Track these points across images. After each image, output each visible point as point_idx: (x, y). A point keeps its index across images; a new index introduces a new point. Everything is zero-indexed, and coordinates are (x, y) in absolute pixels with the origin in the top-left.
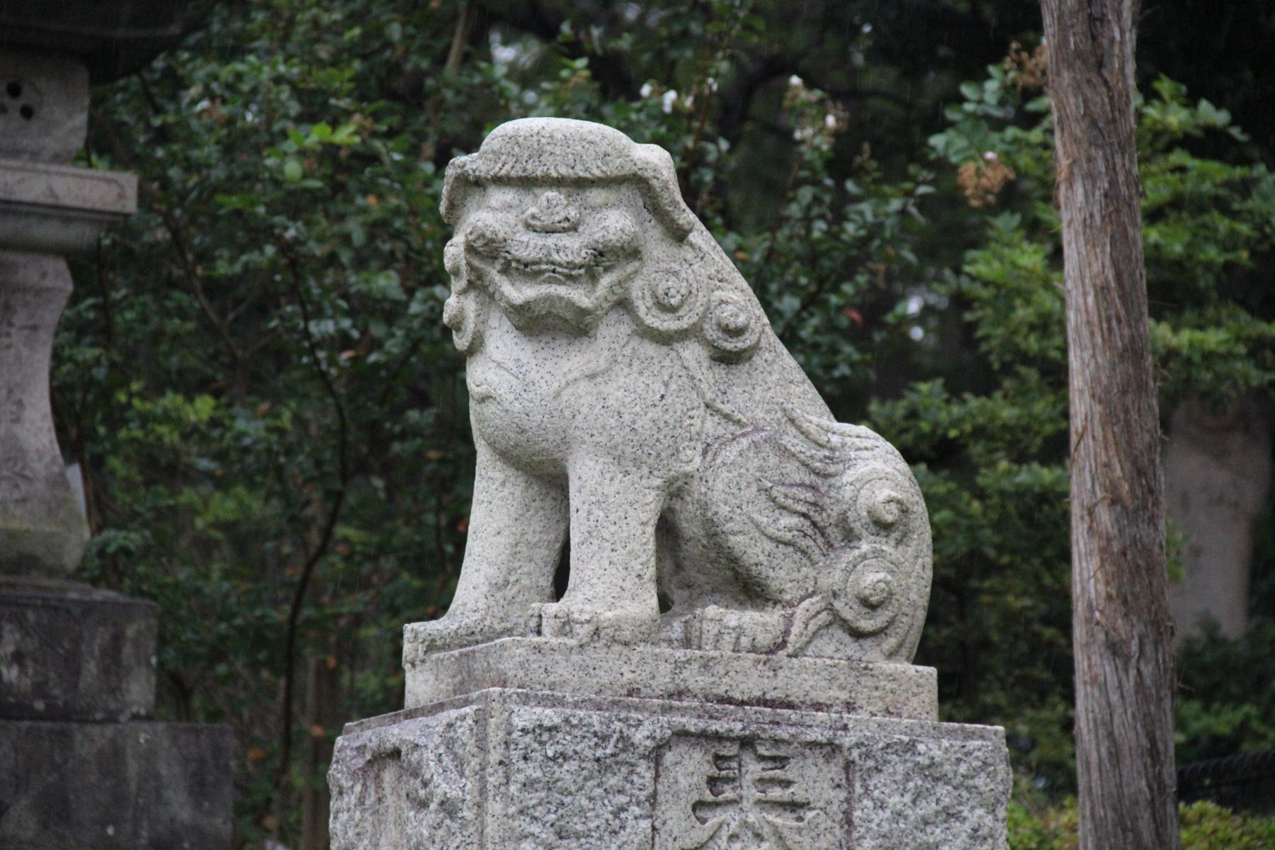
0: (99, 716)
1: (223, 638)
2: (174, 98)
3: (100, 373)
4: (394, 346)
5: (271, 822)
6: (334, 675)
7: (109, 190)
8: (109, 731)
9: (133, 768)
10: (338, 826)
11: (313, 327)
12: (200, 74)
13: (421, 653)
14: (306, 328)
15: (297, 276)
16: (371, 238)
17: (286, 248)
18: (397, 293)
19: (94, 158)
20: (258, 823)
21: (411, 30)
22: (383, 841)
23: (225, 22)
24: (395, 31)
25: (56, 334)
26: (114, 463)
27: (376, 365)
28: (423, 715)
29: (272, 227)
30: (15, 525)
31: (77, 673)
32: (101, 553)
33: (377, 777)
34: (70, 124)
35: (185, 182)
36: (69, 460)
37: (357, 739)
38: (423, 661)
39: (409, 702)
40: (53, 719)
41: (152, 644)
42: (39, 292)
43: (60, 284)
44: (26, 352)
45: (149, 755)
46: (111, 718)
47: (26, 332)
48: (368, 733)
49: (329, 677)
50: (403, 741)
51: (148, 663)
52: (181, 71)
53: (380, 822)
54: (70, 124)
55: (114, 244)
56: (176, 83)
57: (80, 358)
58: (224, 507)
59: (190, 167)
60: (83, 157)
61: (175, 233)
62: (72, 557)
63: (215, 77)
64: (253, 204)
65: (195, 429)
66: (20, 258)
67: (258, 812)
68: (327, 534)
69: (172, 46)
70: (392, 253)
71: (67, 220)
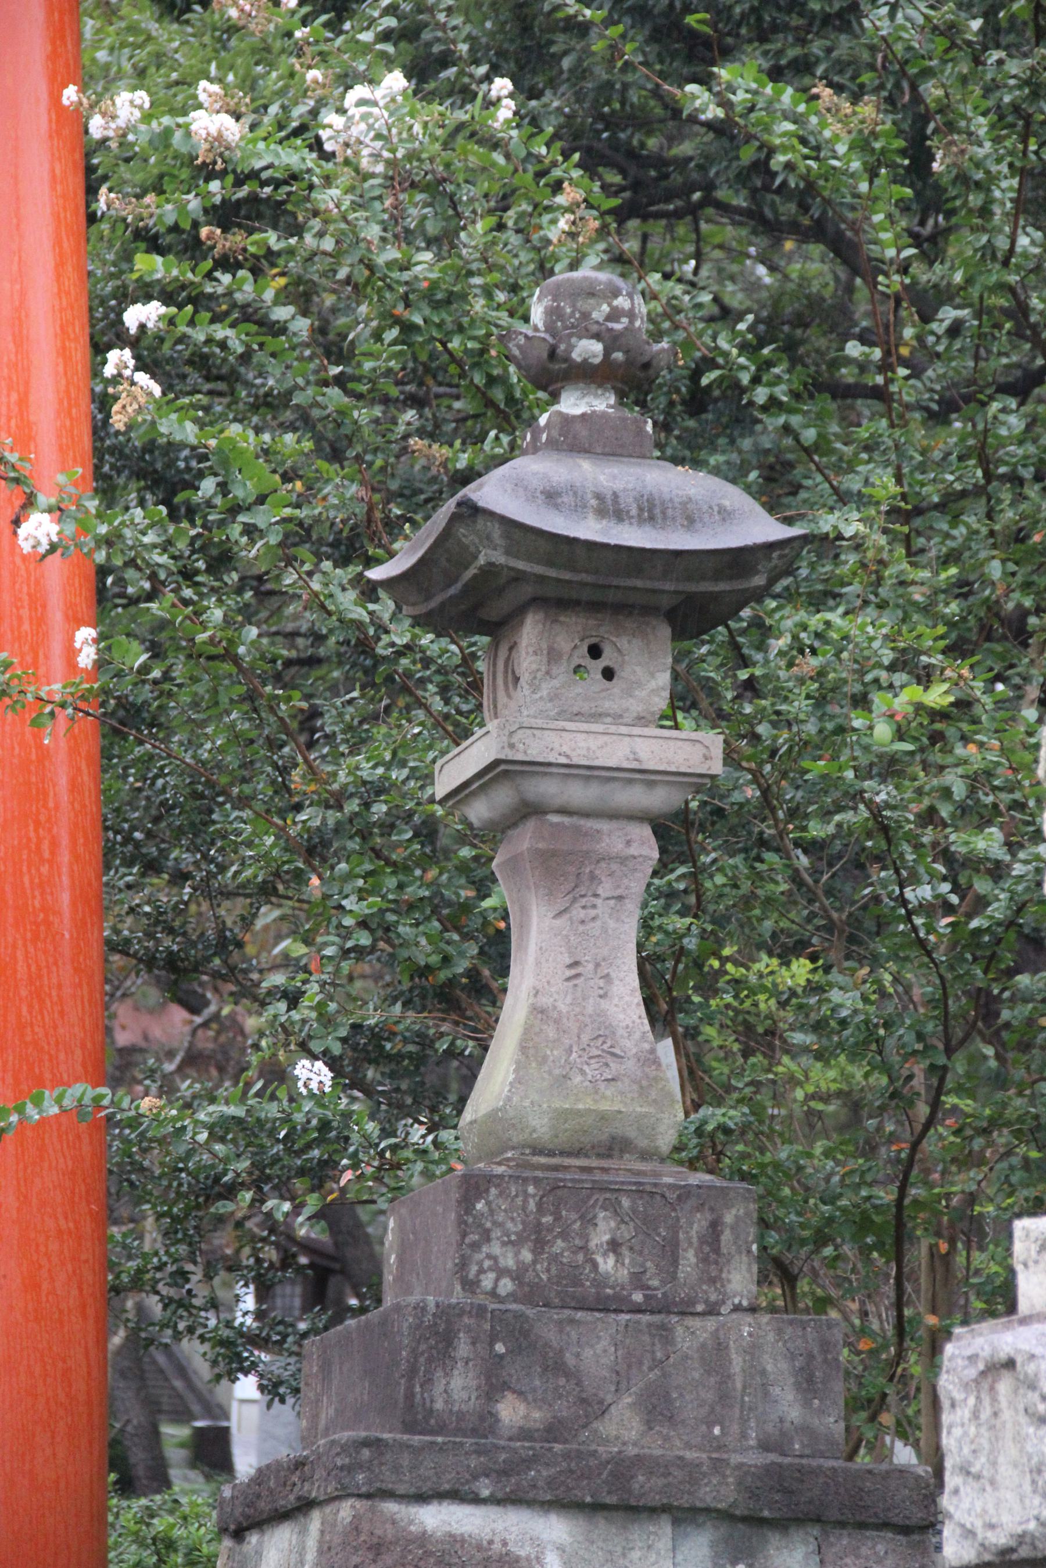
0: (700, 1308)
1: (830, 1220)
2: (761, 646)
3: (691, 943)
4: (998, 910)
5: (887, 1419)
6: (947, 1260)
7: (695, 750)
8: (711, 1323)
9: (737, 1363)
10: (952, 1442)
11: (909, 893)
12: (789, 623)
13: (1033, 1254)
14: (902, 894)
15: (889, 841)
16: (972, 790)
17: (875, 811)
18: (999, 852)
19: (680, 716)
20: (873, 1418)
21: (1011, 567)
22: (1001, 1459)
23: (812, 566)
24: (995, 570)
25: (645, 905)
26: (710, 1031)
27: (978, 932)
28: (1039, 1321)
29: (862, 791)
30: (605, 1106)
31: (675, 1262)
32: (699, 1132)
33: (992, 1389)
34: (653, 684)
35: (775, 739)
36: (659, 1036)
37: (968, 1347)
38: (1036, 1262)
39: (1023, 1306)
40: (652, 1312)
41: (753, 1231)
42: (623, 860)
43: (645, 851)
44: (612, 924)
45: (753, 1350)
46: (712, 1310)
47: (612, 902)
48: (979, 1341)
49: (941, 1263)
50: (1018, 1351)
51: (749, 1251)
52: (768, 622)
53: (997, 1439)
54: (653, 684)
55: (704, 804)
56: (763, 630)
57: (670, 928)
58: (825, 1077)
59: (780, 720)
60: (668, 719)
61: (765, 792)
62: (666, 1140)
63: (805, 627)
64: (840, 769)
65: (793, 993)
66: (604, 826)
67: (875, 1405)
68: (935, 1104)
69: (758, 596)
70: (995, 806)
71: (651, 784)
